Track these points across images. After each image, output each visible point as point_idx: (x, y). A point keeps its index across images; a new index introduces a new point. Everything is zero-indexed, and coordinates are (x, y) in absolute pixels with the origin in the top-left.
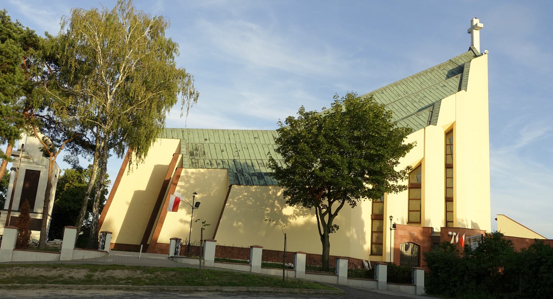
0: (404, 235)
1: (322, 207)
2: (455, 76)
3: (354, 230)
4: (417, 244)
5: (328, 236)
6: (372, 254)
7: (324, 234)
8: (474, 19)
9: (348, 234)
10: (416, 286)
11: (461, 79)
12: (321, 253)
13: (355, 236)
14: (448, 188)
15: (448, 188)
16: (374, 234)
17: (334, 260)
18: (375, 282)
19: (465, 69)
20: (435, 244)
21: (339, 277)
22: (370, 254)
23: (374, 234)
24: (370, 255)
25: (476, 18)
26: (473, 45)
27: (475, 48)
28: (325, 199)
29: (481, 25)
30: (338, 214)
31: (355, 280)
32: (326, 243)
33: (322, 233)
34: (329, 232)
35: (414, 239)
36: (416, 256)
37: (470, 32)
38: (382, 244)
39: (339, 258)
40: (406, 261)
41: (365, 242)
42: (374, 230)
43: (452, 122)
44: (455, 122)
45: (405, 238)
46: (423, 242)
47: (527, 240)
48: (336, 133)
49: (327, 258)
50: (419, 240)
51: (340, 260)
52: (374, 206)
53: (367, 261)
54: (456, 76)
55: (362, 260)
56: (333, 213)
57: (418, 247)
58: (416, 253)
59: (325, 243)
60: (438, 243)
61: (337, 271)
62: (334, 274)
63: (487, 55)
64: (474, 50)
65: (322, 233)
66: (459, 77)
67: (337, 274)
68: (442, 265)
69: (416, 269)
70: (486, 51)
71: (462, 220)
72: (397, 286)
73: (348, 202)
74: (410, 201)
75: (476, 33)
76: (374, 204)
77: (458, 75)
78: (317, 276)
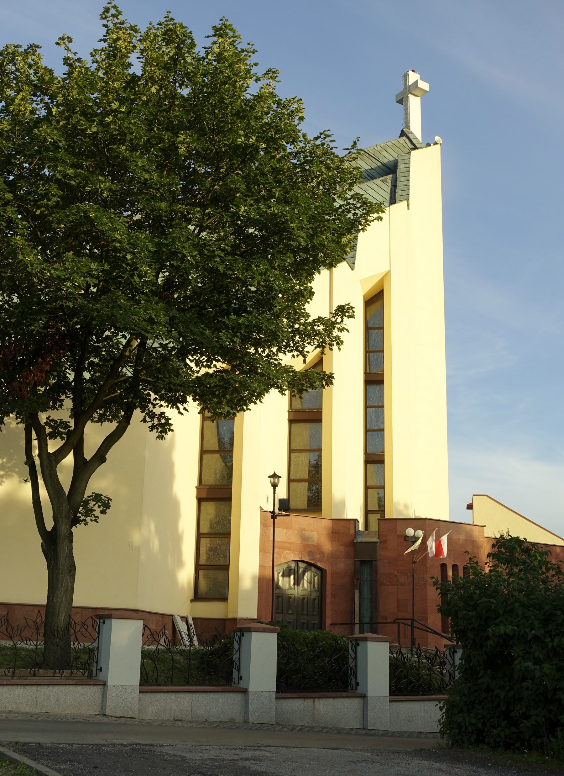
0: (284, 540)
1: (48, 430)
2: (381, 179)
3: (152, 527)
4: (319, 564)
5: (70, 536)
6: (198, 597)
7: (54, 528)
8: (410, 73)
9: (136, 537)
10: (364, 696)
11: (394, 187)
12: (42, 599)
13: (156, 544)
14: (370, 430)
15: (370, 430)
16: (205, 542)
17: (89, 622)
18: (237, 698)
19: (400, 167)
20: (363, 562)
21: (110, 689)
22: (191, 595)
23: (203, 541)
24: (192, 601)
25: (413, 71)
26: (409, 128)
27: (412, 133)
28: (61, 406)
29: (424, 85)
30: (107, 456)
31: (168, 696)
32: (62, 559)
33: (49, 525)
34: (75, 521)
35: (310, 553)
36: (314, 599)
37: (402, 101)
38: (226, 568)
39: (110, 617)
40: (290, 612)
41: (180, 563)
42: (205, 529)
43: (383, 269)
44: (388, 273)
45: (289, 549)
46: (333, 557)
47: (558, 550)
48: (109, 124)
49: (62, 617)
50: (322, 553)
51: (114, 621)
52: (204, 461)
53: (185, 619)
54: (383, 178)
55: (172, 616)
56: (89, 453)
57: (319, 573)
58: (315, 590)
59: (55, 551)
60: (371, 562)
61: (102, 664)
62: (90, 676)
63: (438, 146)
64: (410, 136)
65: (49, 525)
66: (390, 182)
67: (101, 676)
68: (532, 629)
69: (366, 639)
70: (437, 138)
71: (406, 506)
72: (308, 703)
73: (144, 420)
74: (292, 454)
75: (415, 103)
76: (205, 456)
77: (387, 177)
78: (18, 691)
